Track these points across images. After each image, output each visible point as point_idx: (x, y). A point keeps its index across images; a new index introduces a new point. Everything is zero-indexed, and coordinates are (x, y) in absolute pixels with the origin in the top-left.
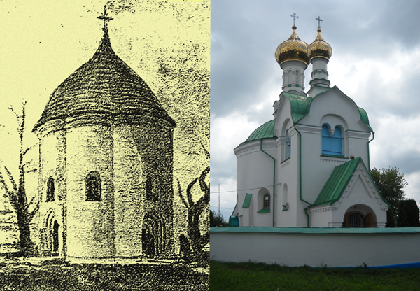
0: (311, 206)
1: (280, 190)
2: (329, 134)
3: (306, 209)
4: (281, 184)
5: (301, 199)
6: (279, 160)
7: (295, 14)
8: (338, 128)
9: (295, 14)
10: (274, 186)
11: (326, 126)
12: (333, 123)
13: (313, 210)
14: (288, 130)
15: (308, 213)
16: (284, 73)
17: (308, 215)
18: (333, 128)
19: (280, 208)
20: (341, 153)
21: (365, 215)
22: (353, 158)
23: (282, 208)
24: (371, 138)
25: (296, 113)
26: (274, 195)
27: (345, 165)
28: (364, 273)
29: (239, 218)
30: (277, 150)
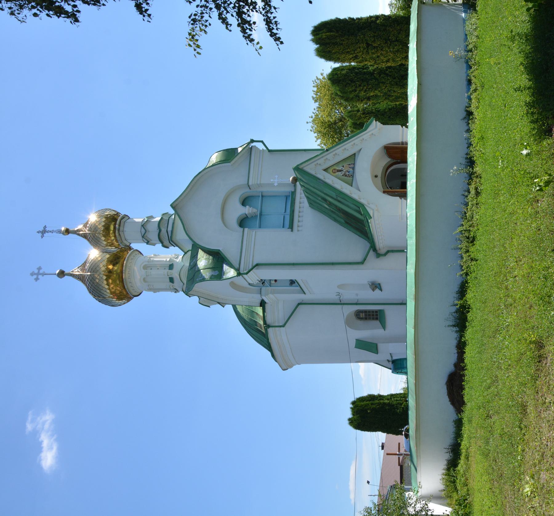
0: (373, 247)
1: (349, 295)
2: (256, 216)
3: (378, 255)
4: (338, 294)
5: (362, 263)
6: (301, 297)
7: (32, 274)
8: (244, 203)
9: (32, 274)
10: (341, 303)
11: (243, 222)
12: (237, 210)
13: (379, 252)
14: (249, 284)
15: (383, 251)
16: (150, 290)
17: (388, 252)
18: (247, 210)
19: (377, 295)
20: (287, 197)
21: (389, 160)
22: (295, 180)
23: (377, 291)
24: (260, 146)
25: (245, 218)
26: (356, 304)
27: (307, 191)
30: (279, 302)
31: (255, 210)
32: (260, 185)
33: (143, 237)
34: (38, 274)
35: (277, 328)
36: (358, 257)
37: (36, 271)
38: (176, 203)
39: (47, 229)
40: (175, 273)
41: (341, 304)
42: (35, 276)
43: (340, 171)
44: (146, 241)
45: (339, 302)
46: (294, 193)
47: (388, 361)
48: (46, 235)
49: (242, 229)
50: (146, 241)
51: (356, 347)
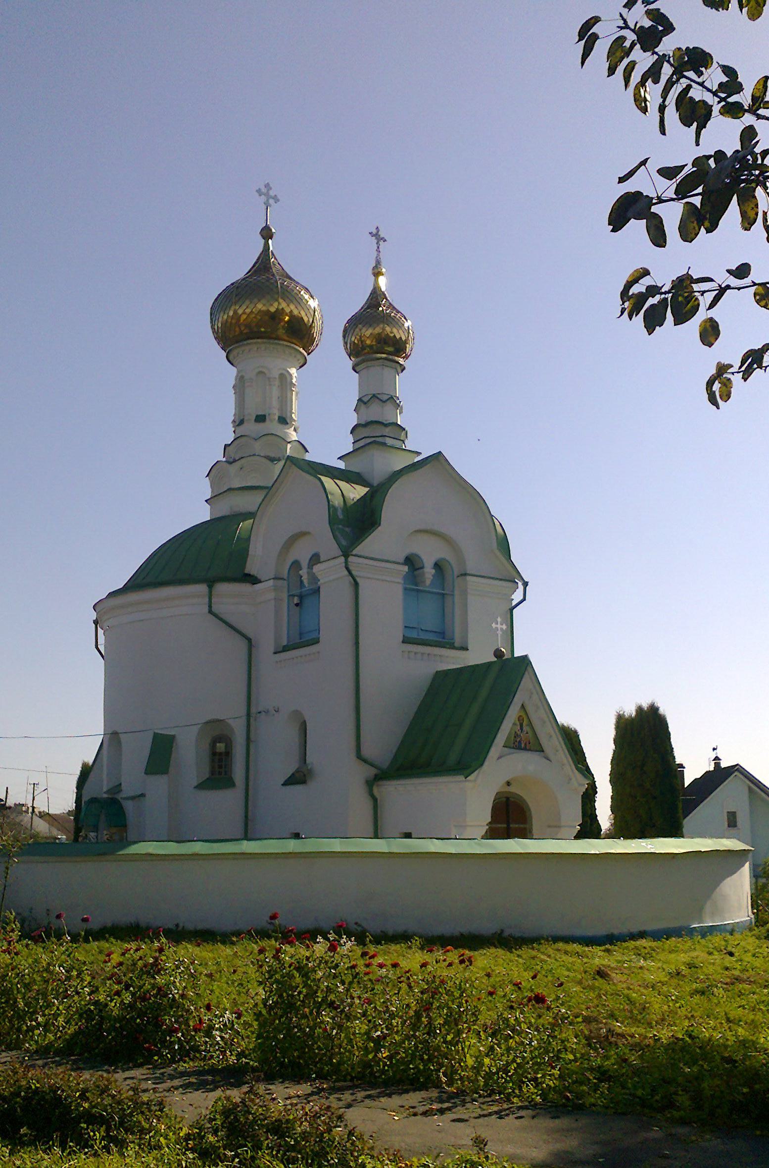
3: (371, 783)
5: (359, 756)
9: (267, 186)
11: (412, 562)
12: (430, 553)
15: (376, 791)
17: (375, 800)
18: (429, 571)
20: (442, 634)
24: (517, 596)
26: (248, 739)
28: (391, 854)
30: (258, 607)
31: (428, 582)
32: (464, 593)
33: (374, 396)
34: (268, 195)
36: (366, 752)
37: (272, 193)
38: (443, 461)
39: (381, 243)
40: (272, 425)
41: (249, 715)
42: (264, 190)
43: (521, 728)
44: (365, 399)
45: (253, 710)
48: (374, 240)
49: (402, 560)
51: (156, 735)
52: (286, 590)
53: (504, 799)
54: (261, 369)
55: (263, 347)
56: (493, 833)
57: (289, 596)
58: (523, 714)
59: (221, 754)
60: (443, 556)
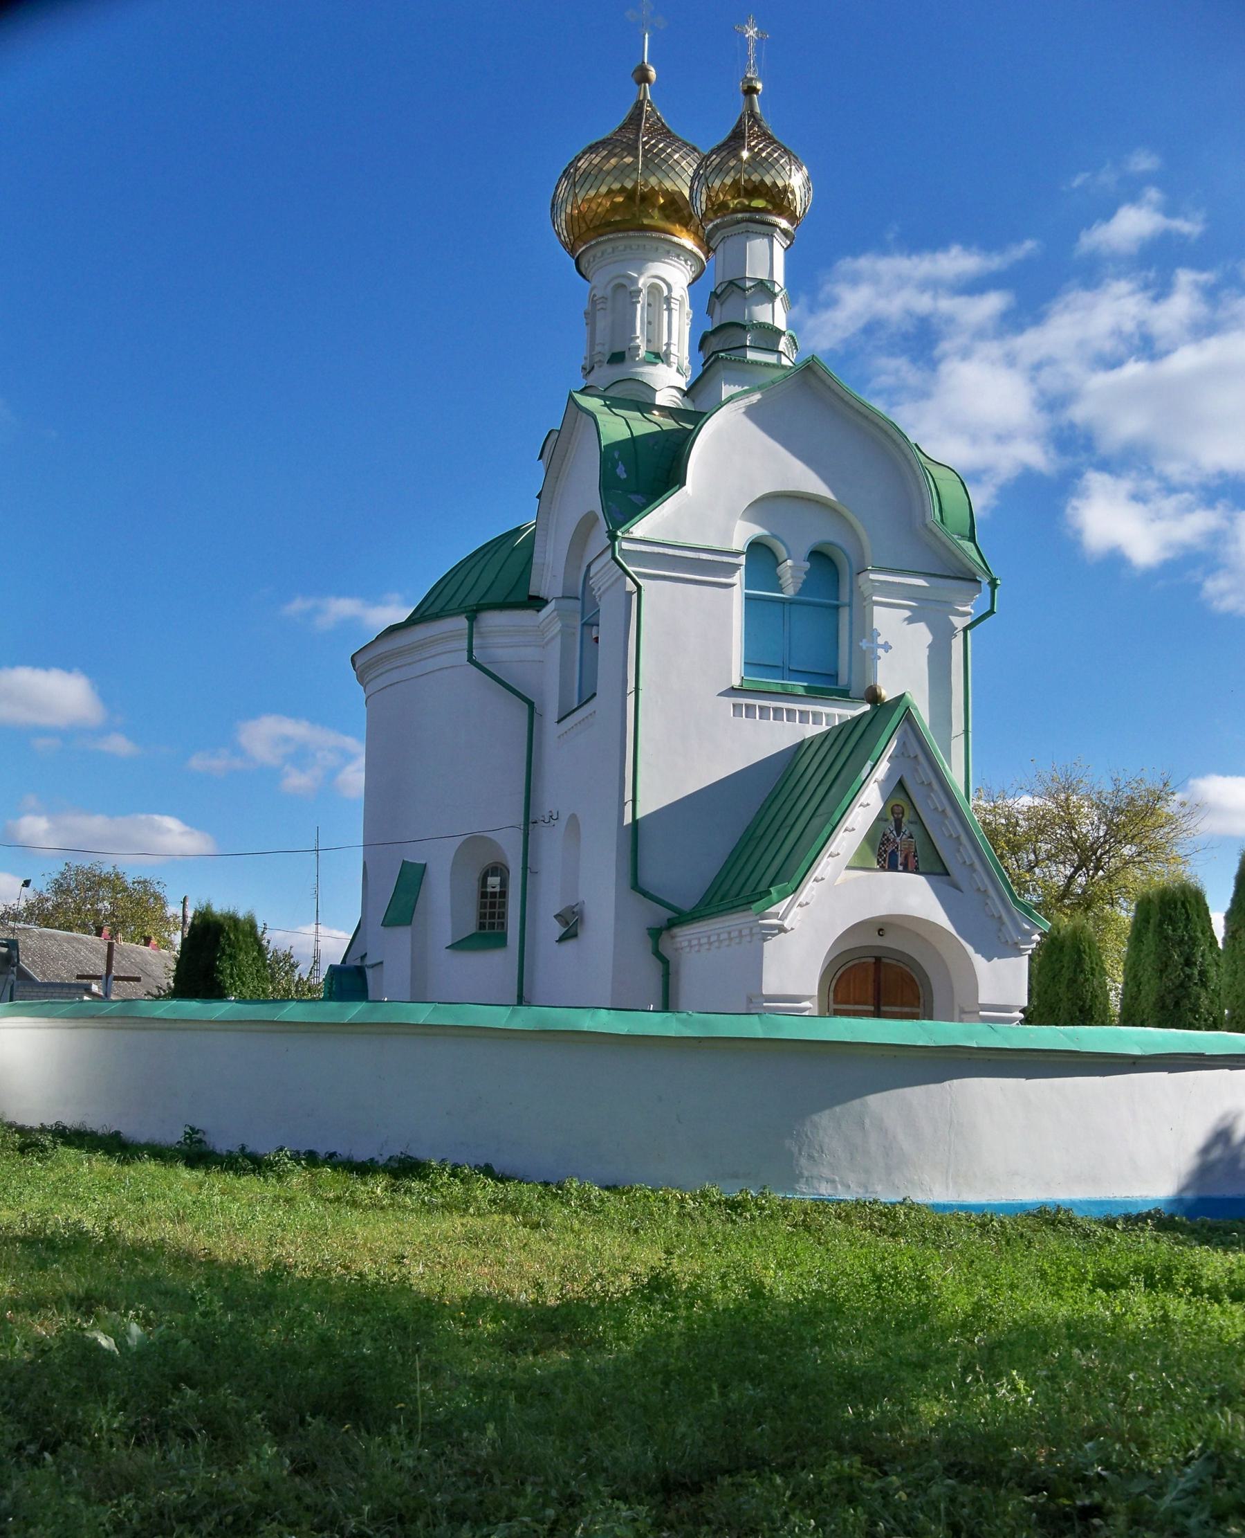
0: (680, 918)
3: (656, 934)
5: (636, 886)
6: (551, 710)
13: (686, 935)
15: (666, 947)
17: (665, 962)
20: (834, 677)
23: (558, 929)
26: (525, 868)
29: (370, 973)
33: (731, 283)
35: (465, 645)
36: (652, 876)
43: (898, 828)
46: (844, 695)
47: (363, 957)
50: (719, 292)
52: (579, 618)
53: (873, 960)
54: (616, 282)
55: (620, 245)
56: (1031, 1017)
57: (583, 625)
58: (900, 800)
59: (493, 895)
60: (831, 537)
